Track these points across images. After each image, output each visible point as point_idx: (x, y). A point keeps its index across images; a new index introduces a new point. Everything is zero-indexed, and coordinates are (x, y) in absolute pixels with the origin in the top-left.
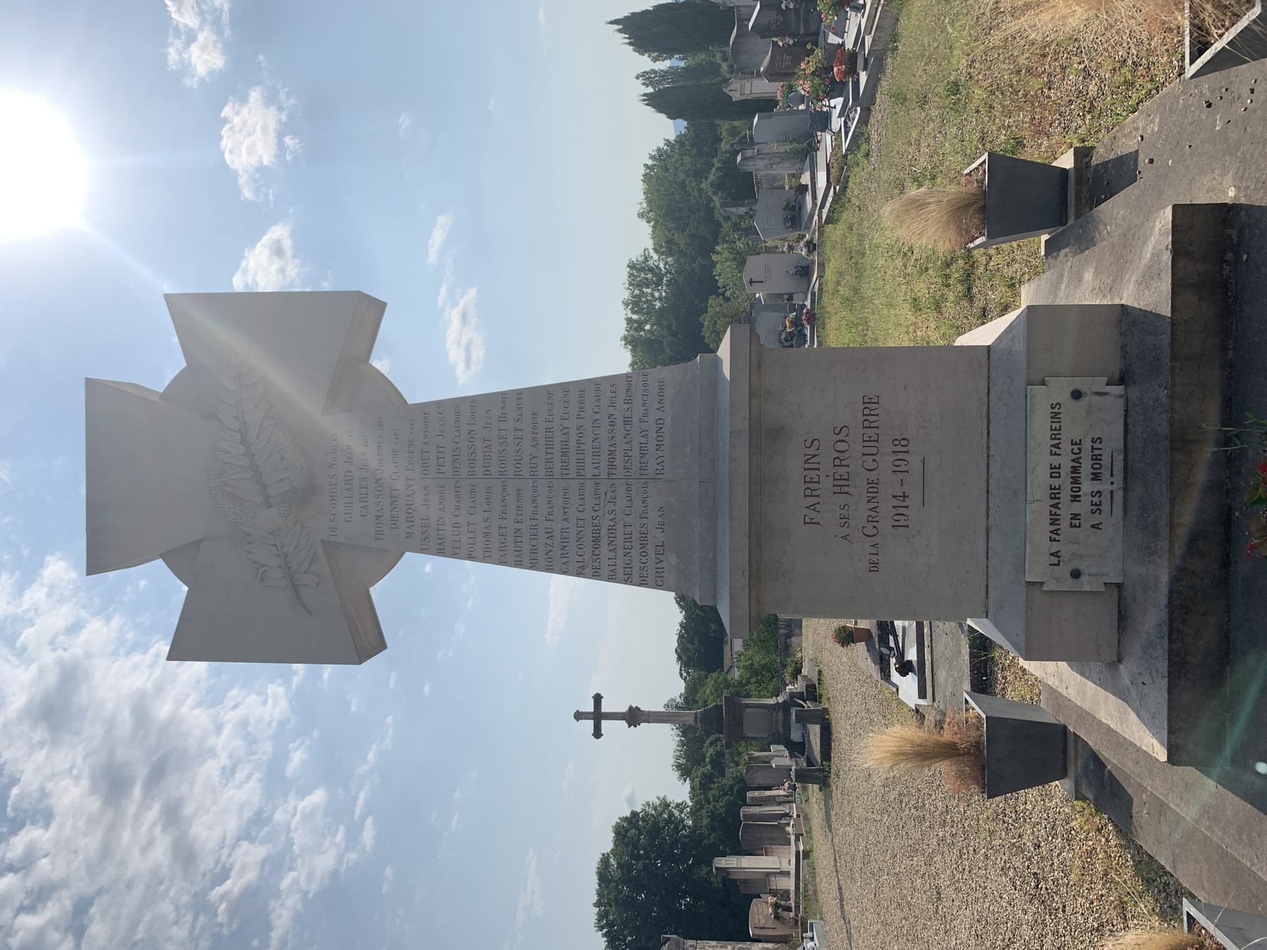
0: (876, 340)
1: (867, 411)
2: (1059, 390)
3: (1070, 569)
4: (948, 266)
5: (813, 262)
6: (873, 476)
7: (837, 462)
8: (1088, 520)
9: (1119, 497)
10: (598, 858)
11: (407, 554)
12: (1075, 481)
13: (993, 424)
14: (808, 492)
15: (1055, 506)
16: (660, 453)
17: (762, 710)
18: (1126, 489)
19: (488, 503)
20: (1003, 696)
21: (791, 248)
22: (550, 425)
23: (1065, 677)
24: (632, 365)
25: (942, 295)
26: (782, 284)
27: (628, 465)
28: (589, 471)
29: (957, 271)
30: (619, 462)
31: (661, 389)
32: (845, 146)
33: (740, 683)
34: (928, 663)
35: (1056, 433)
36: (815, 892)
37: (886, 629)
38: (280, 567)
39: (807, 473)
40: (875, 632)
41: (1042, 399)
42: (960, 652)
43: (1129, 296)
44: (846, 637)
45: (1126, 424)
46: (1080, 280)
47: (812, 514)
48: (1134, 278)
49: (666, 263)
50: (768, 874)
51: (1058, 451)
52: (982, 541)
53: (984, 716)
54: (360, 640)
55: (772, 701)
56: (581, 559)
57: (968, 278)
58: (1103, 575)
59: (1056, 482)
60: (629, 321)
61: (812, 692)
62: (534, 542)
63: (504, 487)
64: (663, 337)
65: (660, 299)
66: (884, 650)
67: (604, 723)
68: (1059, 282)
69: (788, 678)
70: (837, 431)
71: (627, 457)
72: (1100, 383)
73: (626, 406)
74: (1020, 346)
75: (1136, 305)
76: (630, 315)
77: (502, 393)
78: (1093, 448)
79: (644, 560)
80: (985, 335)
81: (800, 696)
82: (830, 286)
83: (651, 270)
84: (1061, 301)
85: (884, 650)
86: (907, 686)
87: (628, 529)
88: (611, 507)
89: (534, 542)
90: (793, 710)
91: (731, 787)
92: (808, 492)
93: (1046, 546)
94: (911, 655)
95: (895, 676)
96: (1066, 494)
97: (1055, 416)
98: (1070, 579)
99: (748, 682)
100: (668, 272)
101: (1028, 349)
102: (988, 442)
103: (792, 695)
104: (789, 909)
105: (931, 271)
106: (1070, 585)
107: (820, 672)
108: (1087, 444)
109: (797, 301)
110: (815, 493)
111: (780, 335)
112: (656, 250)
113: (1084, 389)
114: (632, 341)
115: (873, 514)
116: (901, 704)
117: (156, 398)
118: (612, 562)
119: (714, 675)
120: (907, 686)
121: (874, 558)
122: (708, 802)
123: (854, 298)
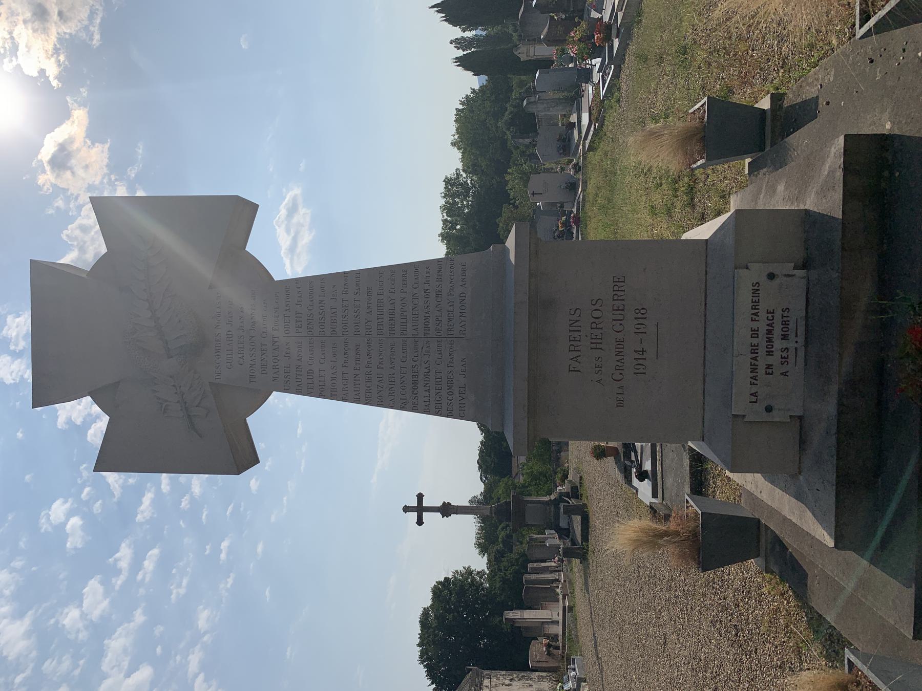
1: (616, 288)
7: (594, 325)
9: (801, 354)
10: (420, 612)
12: (770, 340)
15: (755, 359)
19: (335, 355)
20: (714, 497)
21: (562, 169)
24: (447, 254)
25: (673, 203)
31: (464, 271)
34: (659, 472)
35: (755, 305)
37: (629, 448)
38: (178, 402)
43: (810, 203)
44: (600, 453)
46: (775, 191)
49: (472, 180)
54: (240, 456)
55: (546, 499)
59: (755, 341)
60: (445, 221)
61: (575, 493)
65: (467, 206)
66: (627, 463)
67: (426, 515)
68: (759, 192)
69: (558, 481)
70: (594, 302)
72: (789, 268)
77: (344, 272)
80: (704, 232)
81: (567, 495)
83: (462, 185)
85: (627, 463)
86: (644, 489)
90: (562, 505)
91: (517, 560)
94: (647, 466)
95: (636, 482)
96: (762, 351)
97: (755, 292)
98: (765, 413)
99: (530, 485)
100: (474, 186)
103: (561, 494)
105: (664, 186)
107: (581, 477)
108: (778, 315)
109: (567, 208)
112: (464, 171)
114: (444, 237)
115: (620, 364)
117: (84, 276)
119: (505, 479)
120: (644, 489)
121: (620, 396)
122: (500, 570)
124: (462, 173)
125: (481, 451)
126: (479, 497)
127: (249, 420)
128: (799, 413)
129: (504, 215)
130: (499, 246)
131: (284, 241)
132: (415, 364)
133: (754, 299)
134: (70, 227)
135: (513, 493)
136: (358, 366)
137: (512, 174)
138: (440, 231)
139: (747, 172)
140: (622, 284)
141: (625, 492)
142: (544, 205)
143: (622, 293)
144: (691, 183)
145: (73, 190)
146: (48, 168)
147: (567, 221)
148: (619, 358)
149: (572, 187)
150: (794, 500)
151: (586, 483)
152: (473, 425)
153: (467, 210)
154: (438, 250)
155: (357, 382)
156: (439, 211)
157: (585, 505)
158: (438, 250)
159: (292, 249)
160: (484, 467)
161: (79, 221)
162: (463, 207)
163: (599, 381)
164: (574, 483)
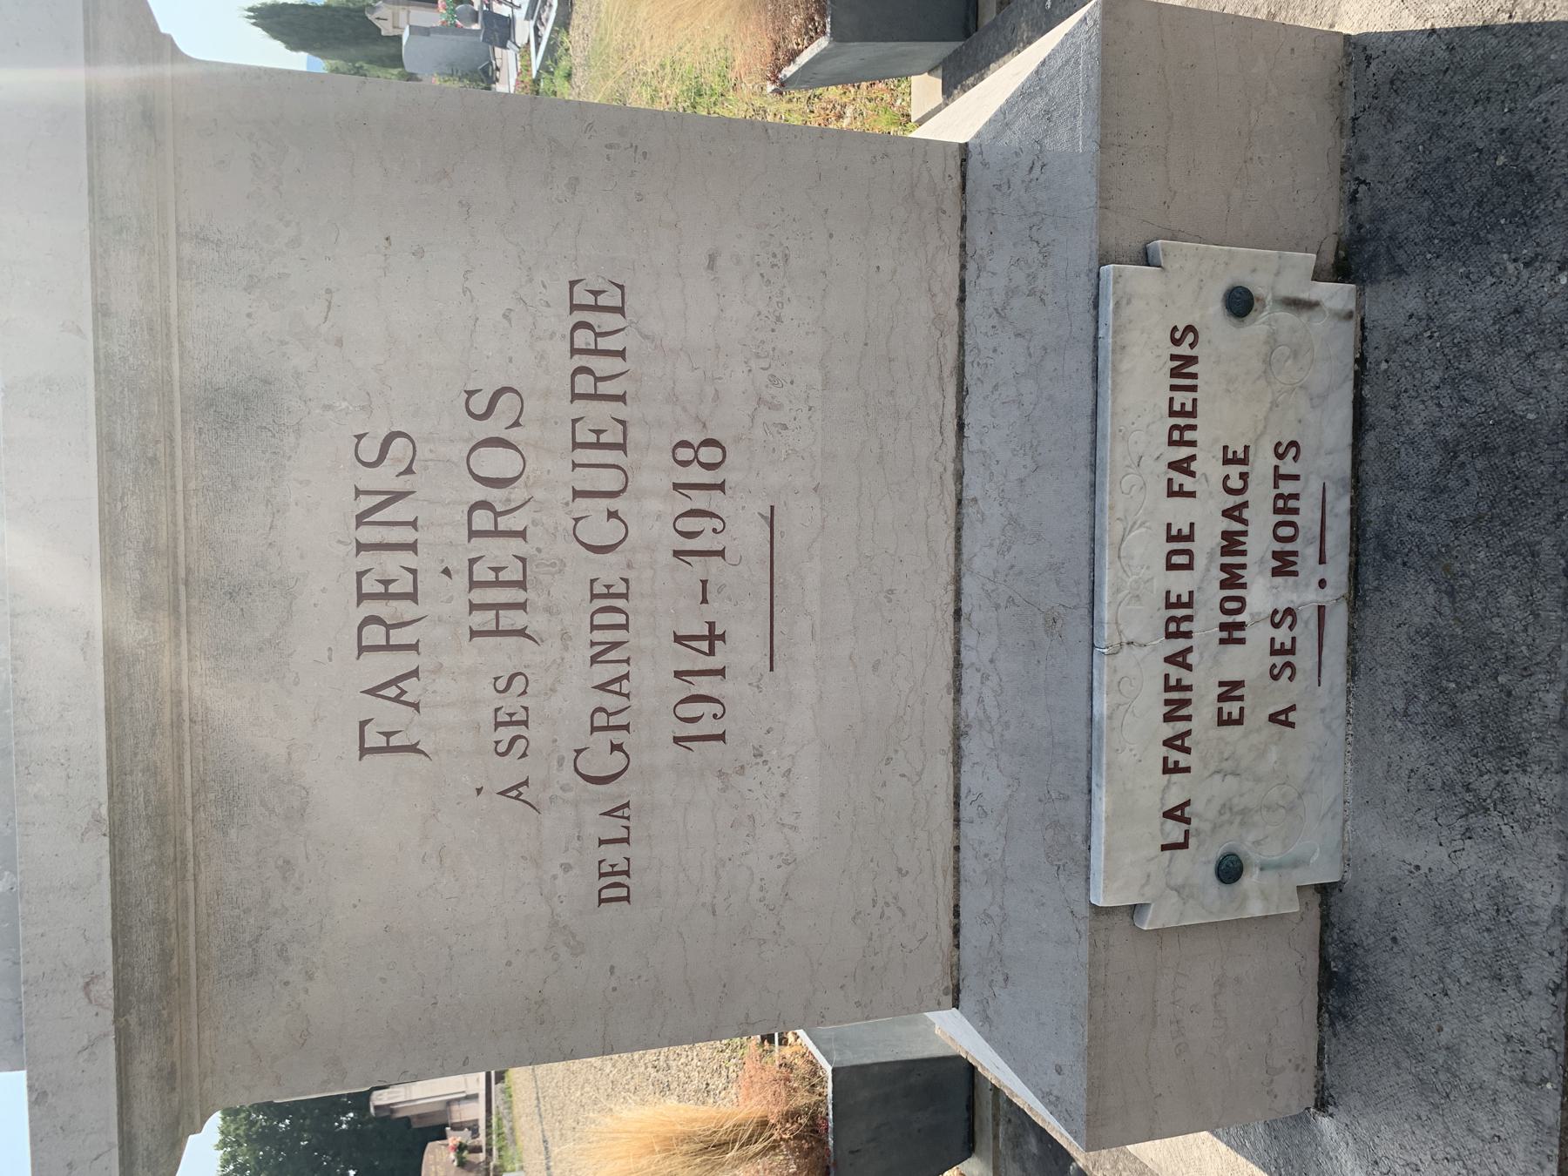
1: (584, 338)
2: (1182, 288)
3: (1215, 853)
6: (608, 569)
7: (483, 520)
8: (1261, 701)
12: (1232, 579)
13: (973, 401)
14: (374, 635)
18: (1357, 597)
32: (536, 63)
36: (512, 1129)
39: (366, 560)
41: (1182, 288)
45: (1359, 404)
47: (387, 714)
50: (449, 1103)
51: (1189, 484)
53: (828, 1069)
58: (1296, 863)
59: (1180, 583)
74: (1075, 137)
75: (1409, 23)
78: (1278, 477)
92: (374, 635)
93: (1155, 791)
96: (1206, 622)
97: (1182, 368)
98: (1213, 886)
101: (1103, 146)
102: (959, 458)
104: (477, 1150)
106: (1213, 902)
108: (1263, 463)
110: (398, 637)
113: (1259, 286)
115: (612, 702)
121: (614, 854)
125: (305, 6)
148: (604, 673)
163: (514, 792)
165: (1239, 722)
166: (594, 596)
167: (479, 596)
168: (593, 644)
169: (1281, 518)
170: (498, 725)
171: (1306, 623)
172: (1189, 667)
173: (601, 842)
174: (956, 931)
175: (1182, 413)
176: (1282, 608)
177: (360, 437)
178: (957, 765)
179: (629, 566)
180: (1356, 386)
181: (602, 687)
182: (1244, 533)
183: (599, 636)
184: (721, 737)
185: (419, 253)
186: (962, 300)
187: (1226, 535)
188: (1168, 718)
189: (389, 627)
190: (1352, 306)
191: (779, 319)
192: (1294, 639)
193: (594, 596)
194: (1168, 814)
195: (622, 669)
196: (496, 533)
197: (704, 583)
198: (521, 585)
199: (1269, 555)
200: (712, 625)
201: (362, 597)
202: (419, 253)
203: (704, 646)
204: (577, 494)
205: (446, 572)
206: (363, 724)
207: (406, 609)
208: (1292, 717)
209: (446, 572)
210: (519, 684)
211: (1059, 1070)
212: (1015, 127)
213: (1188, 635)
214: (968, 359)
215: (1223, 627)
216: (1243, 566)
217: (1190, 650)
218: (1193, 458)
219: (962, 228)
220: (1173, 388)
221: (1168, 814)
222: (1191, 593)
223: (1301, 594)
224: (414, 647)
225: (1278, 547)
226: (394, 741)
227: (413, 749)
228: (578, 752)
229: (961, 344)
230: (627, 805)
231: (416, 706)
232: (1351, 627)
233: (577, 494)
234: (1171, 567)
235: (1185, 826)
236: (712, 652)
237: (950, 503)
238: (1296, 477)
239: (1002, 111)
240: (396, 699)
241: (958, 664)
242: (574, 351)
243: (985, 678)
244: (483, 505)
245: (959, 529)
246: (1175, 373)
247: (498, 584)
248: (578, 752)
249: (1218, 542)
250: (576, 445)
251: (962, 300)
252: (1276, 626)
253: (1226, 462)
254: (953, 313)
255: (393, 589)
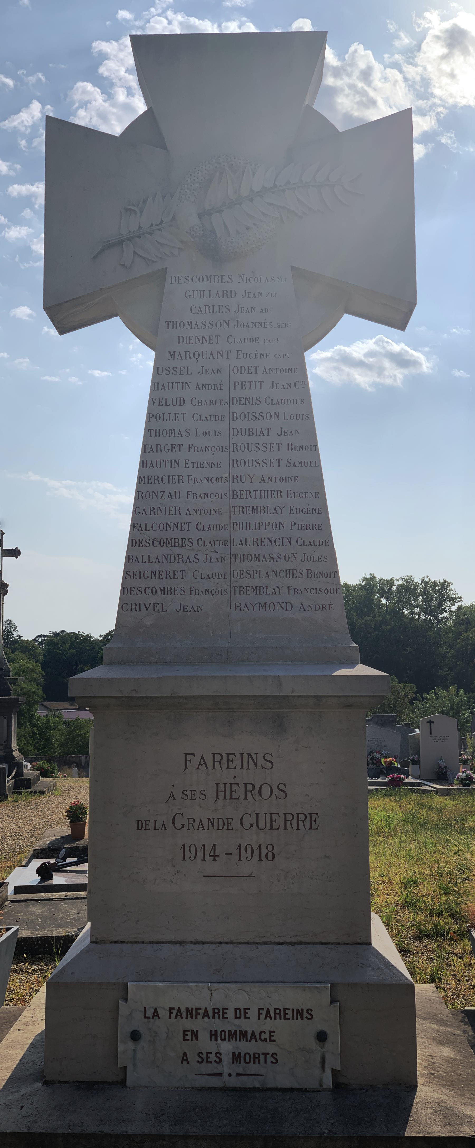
0: (374, 845)
1: (302, 817)
3: (142, 1030)
4: (452, 916)
5: (451, 784)
6: (235, 824)
7: (249, 787)
9: (215, 1082)
11: (153, 353)
12: (232, 1035)
14: (218, 758)
15: (206, 1014)
16: (257, 607)
17: (5, 735)
18: (224, 1090)
19: (205, 433)
20: (15, 971)
21: (465, 762)
22: (285, 494)
23: (30, 1028)
24: (346, 586)
25: (421, 910)
26: (429, 752)
27: (245, 574)
28: (238, 535)
29: (446, 923)
30: (247, 565)
31: (322, 608)
33: (33, 716)
34: (49, 895)
35: (281, 1013)
37: (82, 855)
38: (140, 228)
39: (238, 756)
40: (81, 843)
41: (316, 1000)
42: (60, 926)
43: (426, 1093)
44: (75, 815)
45: (291, 1090)
46: (442, 1043)
47: (196, 760)
48: (445, 1098)
49: (447, 619)
51: (263, 1016)
52: (169, 937)
54: (67, 310)
55: (14, 745)
56: (149, 527)
57: (439, 934)
58: (134, 1065)
59: (230, 1014)
60: (391, 583)
61: (23, 785)
62: (165, 480)
63: (221, 449)
64: (374, 616)
65: (412, 613)
66: (63, 852)
68: (440, 1022)
69: (38, 764)
70: (282, 787)
71: (252, 574)
72: (334, 1062)
73: (305, 572)
74: (371, 976)
75: (416, 1100)
76: (397, 583)
77: (316, 446)
79: (148, 591)
80: (382, 941)
81: (20, 773)
82: (427, 801)
83: (441, 604)
84: (419, 1024)
85: (63, 852)
86: (27, 875)
87: (179, 575)
88: (202, 557)
89: (165, 480)
90: (5, 766)
92: (218, 758)
94: (58, 879)
95: (36, 863)
96: (217, 1025)
97: (299, 1014)
98: (129, 1029)
99: (34, 725)
100: (439, 621)
102: (271, 943)
103: (20, 766)
105: (444, 898)
107: (42, 793)
108: (270, 1048)
109: (412, 768)
110: (217, 764)
111: (378, 752)
112: (460, 608)
114: (370, 584)
115: (196, 824)
116: (10, 870)
117: (307, 102)
118: (146, 559)
119: (40, 692)
120: (27, 875)
121: (151, 825)
123: (415, 824)
124: (457, 605)
125: (77, 636)
126: (15, 634)
127: (117, 321)
128: (128, 1083)
129: (402, 685)
130: (357, 655)
131: (358, 350)
132: (195, 543)
133: (290, 1012)
134: (370, 53)
135: (22, 699)
136: (191, 465)
137: (457, 696)
138: (378, 577)
139: (466, 1008)
140: (308, 826)
141: (22, 851)
142: (416, 739)
143: (295, 827)
144: (451, 933)
145: (420, 58)
146: (447, 25)
147: (394, 769)
148: (205, 822)
149: (441, 775)
150: (8, 1075)
151: (35, 800)
152: (110, 625)
153: (406, 612)
154: (351, 573)
155: (168, 464)
156: (405, 574)
157: (6, 798)
158: (351, 573)
159: (347, 360)
160: (56, 639)
161: (377, 67)
162: (411, 607)
164: (35, 783)
165: (185, 1039)
166: (228, 819)
167: (228, 786)
168: (214, 819)
169: (252, 1056)
170: (191, 791)
171: (216, 1068)
172: (203, 1018)
173: (155, 821)
174: (116, 942)
175: (285, 1014)
176: (222, 1057)
177: (271, 755)
178: (171, 943)
179: (237, 830)
180: (297, 1089)
181: (201, 822)
182: (247, 1041)
183: (216, 821)
184: (184, 859)
185: (322, 771)
186: (322, 943)
187: (246, 1032)
188: (187, 1009)
189: (220, 762)
190: (325, 1087)
191: (312, 879)
192: (211, 1062)
193: (228, 819)
194: (156, 1010)
195: (206, 828)
196: (246, 791)
197: (231, 854)
198: (231, 798)
199: (240, 1051)
200: (218, 856)
201: (228, 755)
202: (322, 771)
203: (212, 854)
204: (257, 815)
205: (235, 777)
206: (194, 754)
207: (225, 766)
208: (185, 1062)
209: (235, 777)
210: (203, 797)
211: (73, 973)
212: (375, 959)
213: (214, 1017)
214: (303, 946)
215: (216, 1031)
216: (236, 1040)
217: (209, 1018)
218: (271, 1018)
219: (345, 943)
220: (293, 1010)
221: (156, 1010)
222: (227, 1018)
223: (226, 1067)
224: (214, 768)
225: (242, 1055)
226: (188, 763)
227: (186, 768)
228: (182, 814)
229: (308, 943)
230: (165, 829)
231: (198, 768)
232: (215, 1088)
233: (257, 815)
234: (236, 1009)
235: (151, 1017)
236: (210, 856)
237: (257, 940)
238: (266, 1063)
239: (381, 955)
240: (200, 763)
241: (204, 943)
242: (298, 814)
243: (200, 952)
244: (222, 756)
245: (248, 943)
246: (298, 1010)
247: (232, 791)
248: (182, 814)
249: (244, 1029)
250: (271, 814)
251: (322, 943)
252: (216, 1054)
253: (270, 1032)
254: (317, 941)
255: (230, 763)
